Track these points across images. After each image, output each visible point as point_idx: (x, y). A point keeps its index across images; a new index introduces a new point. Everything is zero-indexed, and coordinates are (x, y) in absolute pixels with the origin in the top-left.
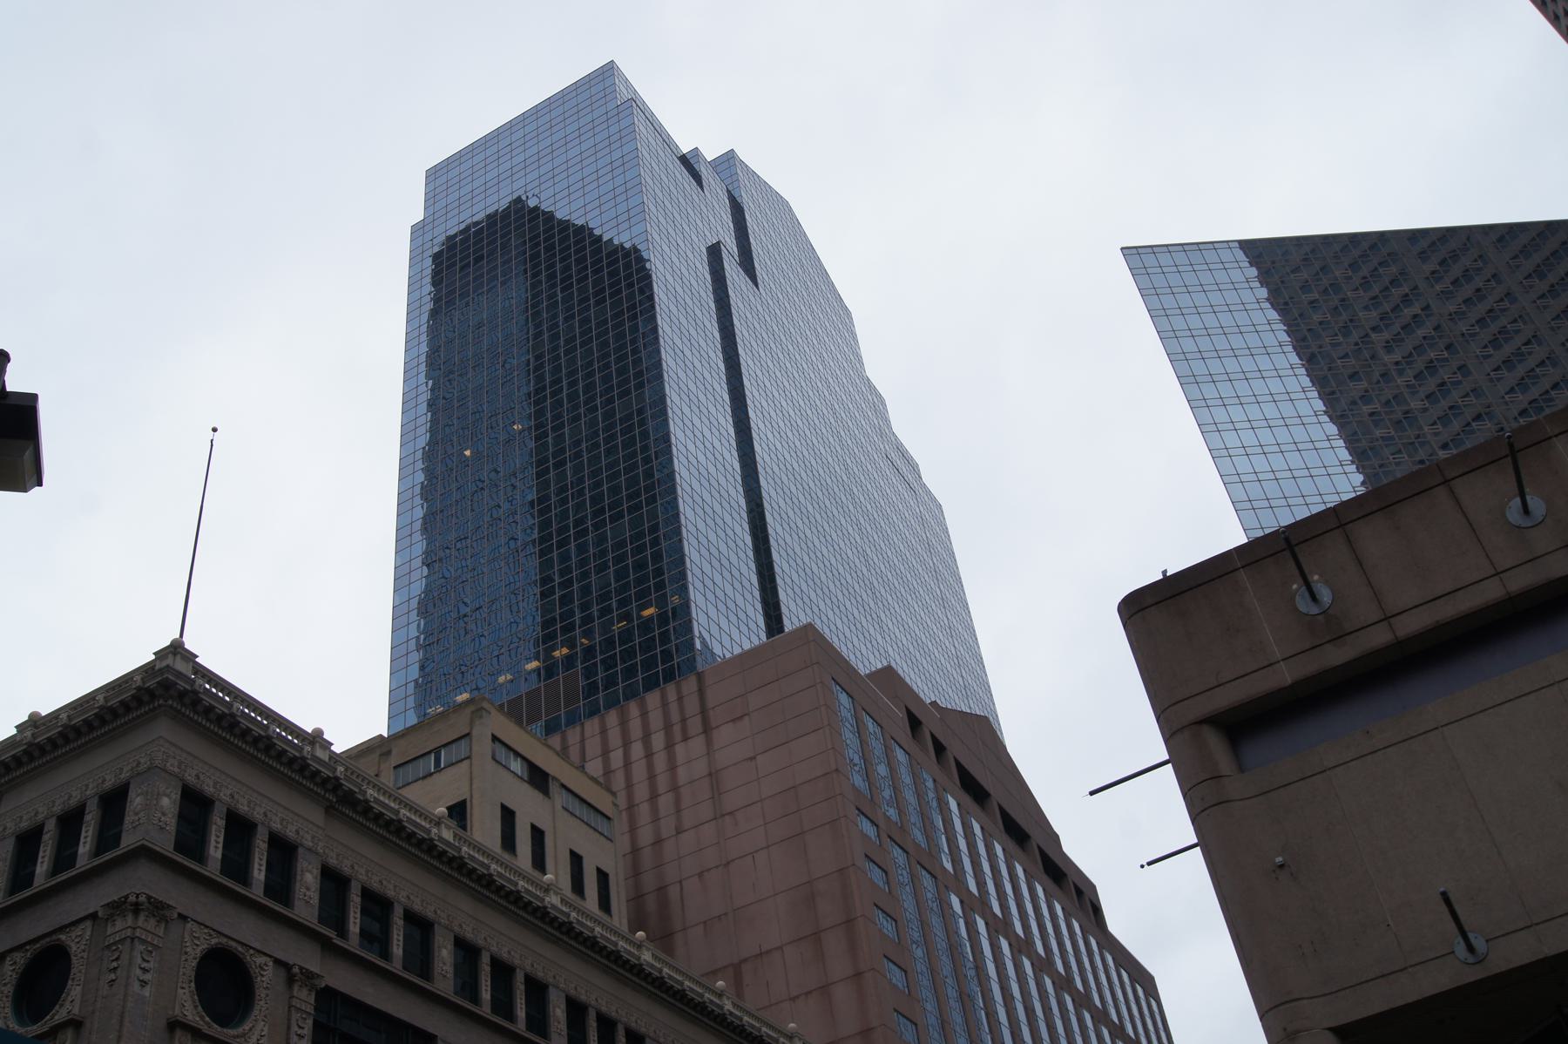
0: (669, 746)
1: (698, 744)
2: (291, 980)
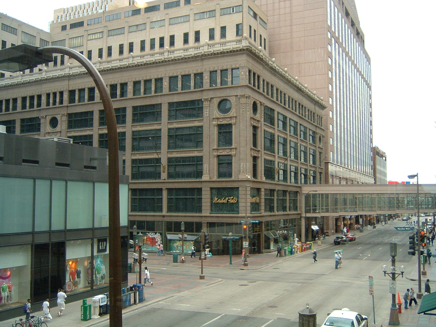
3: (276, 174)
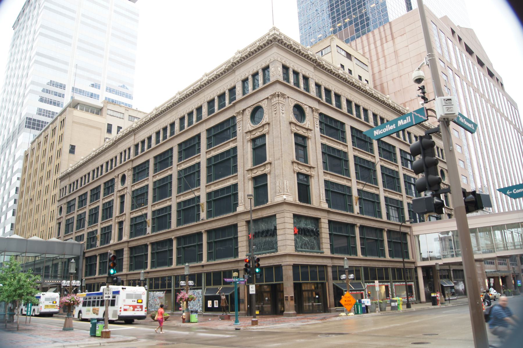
0: (382, 44)
1: (390, 43)
2: (313, 111)
3: (354, 204)
